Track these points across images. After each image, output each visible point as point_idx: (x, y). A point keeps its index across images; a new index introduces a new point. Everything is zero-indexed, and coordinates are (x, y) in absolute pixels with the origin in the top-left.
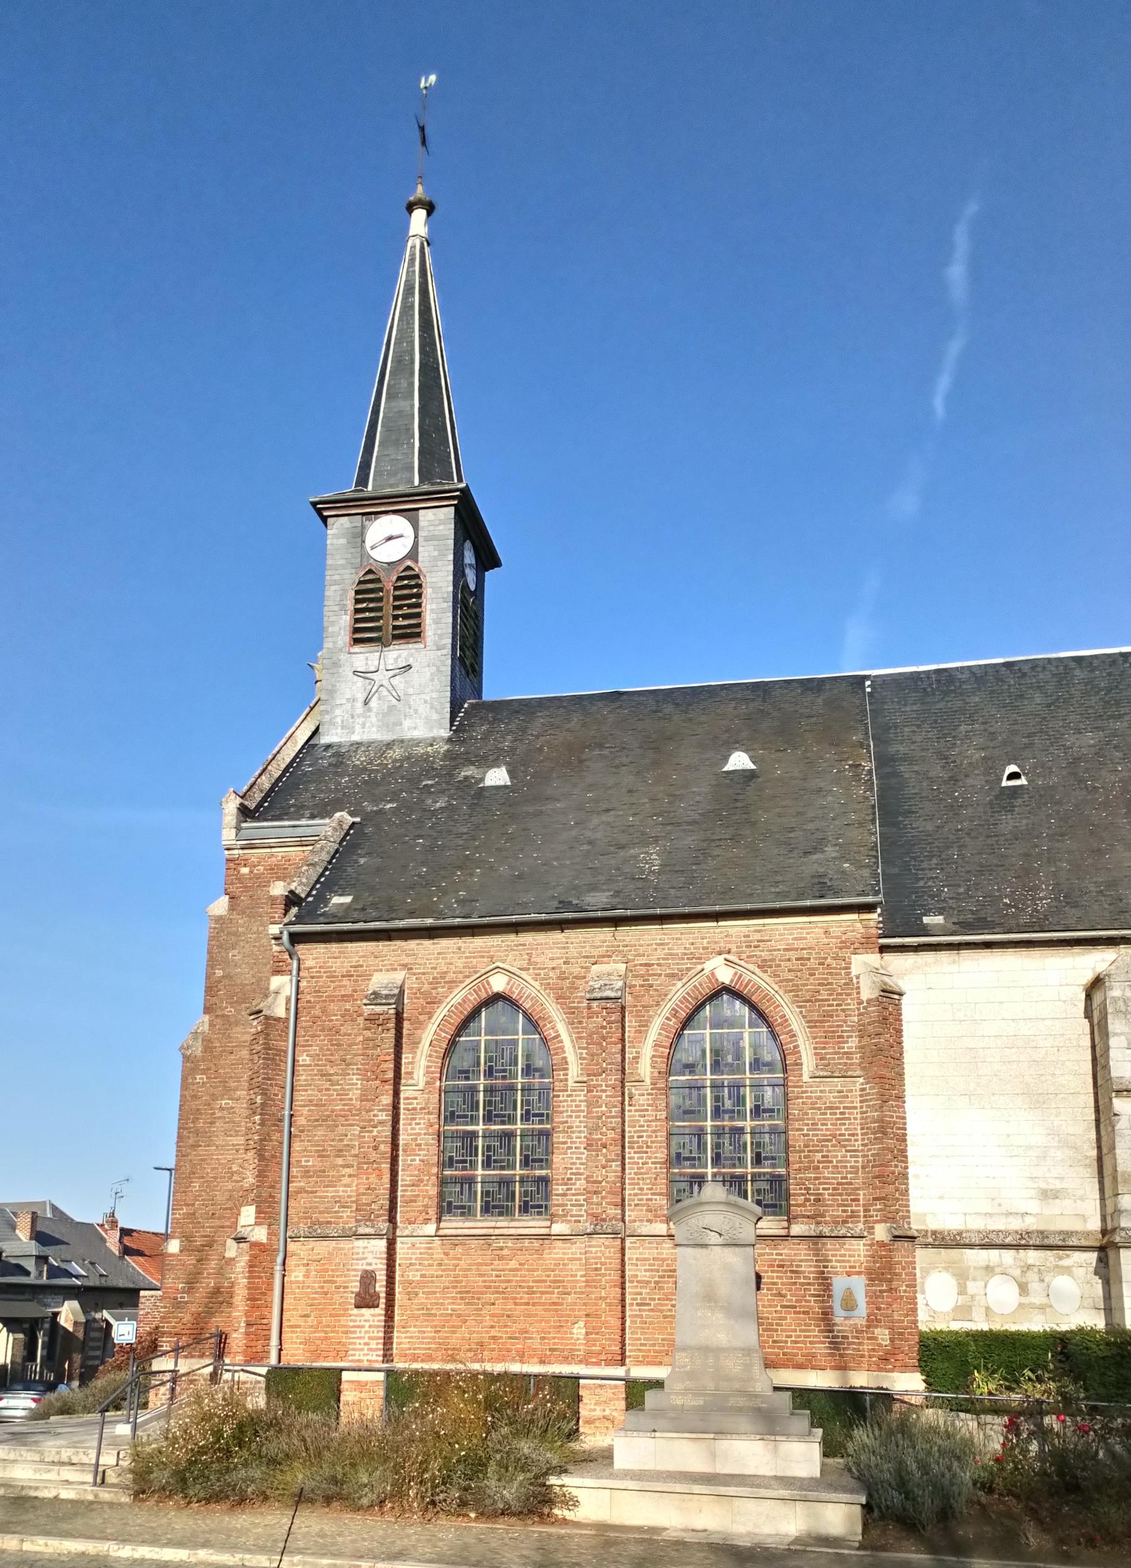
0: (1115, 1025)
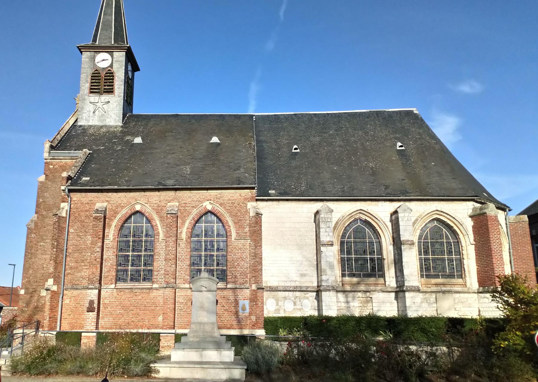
0: (322, 225)
